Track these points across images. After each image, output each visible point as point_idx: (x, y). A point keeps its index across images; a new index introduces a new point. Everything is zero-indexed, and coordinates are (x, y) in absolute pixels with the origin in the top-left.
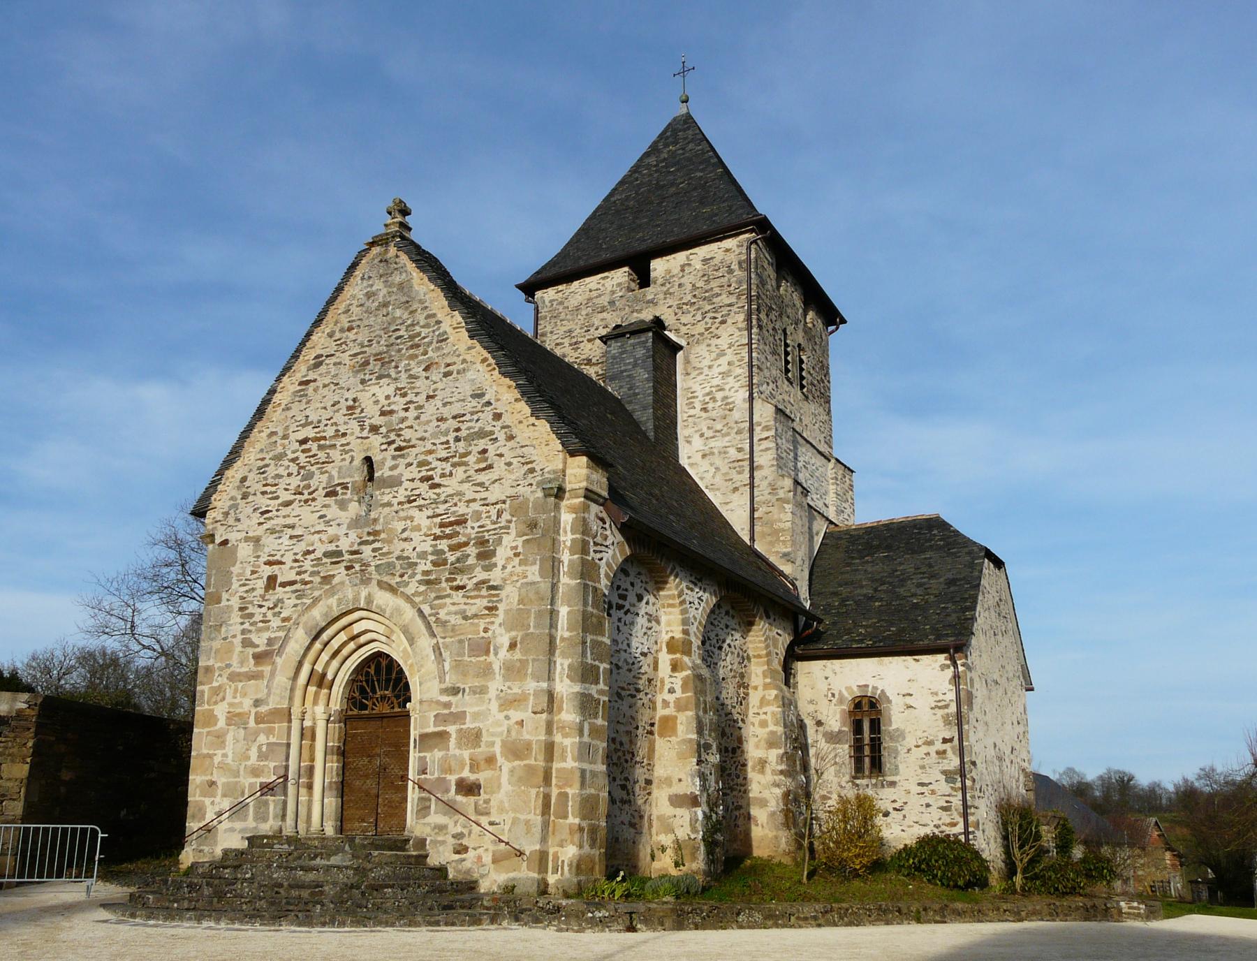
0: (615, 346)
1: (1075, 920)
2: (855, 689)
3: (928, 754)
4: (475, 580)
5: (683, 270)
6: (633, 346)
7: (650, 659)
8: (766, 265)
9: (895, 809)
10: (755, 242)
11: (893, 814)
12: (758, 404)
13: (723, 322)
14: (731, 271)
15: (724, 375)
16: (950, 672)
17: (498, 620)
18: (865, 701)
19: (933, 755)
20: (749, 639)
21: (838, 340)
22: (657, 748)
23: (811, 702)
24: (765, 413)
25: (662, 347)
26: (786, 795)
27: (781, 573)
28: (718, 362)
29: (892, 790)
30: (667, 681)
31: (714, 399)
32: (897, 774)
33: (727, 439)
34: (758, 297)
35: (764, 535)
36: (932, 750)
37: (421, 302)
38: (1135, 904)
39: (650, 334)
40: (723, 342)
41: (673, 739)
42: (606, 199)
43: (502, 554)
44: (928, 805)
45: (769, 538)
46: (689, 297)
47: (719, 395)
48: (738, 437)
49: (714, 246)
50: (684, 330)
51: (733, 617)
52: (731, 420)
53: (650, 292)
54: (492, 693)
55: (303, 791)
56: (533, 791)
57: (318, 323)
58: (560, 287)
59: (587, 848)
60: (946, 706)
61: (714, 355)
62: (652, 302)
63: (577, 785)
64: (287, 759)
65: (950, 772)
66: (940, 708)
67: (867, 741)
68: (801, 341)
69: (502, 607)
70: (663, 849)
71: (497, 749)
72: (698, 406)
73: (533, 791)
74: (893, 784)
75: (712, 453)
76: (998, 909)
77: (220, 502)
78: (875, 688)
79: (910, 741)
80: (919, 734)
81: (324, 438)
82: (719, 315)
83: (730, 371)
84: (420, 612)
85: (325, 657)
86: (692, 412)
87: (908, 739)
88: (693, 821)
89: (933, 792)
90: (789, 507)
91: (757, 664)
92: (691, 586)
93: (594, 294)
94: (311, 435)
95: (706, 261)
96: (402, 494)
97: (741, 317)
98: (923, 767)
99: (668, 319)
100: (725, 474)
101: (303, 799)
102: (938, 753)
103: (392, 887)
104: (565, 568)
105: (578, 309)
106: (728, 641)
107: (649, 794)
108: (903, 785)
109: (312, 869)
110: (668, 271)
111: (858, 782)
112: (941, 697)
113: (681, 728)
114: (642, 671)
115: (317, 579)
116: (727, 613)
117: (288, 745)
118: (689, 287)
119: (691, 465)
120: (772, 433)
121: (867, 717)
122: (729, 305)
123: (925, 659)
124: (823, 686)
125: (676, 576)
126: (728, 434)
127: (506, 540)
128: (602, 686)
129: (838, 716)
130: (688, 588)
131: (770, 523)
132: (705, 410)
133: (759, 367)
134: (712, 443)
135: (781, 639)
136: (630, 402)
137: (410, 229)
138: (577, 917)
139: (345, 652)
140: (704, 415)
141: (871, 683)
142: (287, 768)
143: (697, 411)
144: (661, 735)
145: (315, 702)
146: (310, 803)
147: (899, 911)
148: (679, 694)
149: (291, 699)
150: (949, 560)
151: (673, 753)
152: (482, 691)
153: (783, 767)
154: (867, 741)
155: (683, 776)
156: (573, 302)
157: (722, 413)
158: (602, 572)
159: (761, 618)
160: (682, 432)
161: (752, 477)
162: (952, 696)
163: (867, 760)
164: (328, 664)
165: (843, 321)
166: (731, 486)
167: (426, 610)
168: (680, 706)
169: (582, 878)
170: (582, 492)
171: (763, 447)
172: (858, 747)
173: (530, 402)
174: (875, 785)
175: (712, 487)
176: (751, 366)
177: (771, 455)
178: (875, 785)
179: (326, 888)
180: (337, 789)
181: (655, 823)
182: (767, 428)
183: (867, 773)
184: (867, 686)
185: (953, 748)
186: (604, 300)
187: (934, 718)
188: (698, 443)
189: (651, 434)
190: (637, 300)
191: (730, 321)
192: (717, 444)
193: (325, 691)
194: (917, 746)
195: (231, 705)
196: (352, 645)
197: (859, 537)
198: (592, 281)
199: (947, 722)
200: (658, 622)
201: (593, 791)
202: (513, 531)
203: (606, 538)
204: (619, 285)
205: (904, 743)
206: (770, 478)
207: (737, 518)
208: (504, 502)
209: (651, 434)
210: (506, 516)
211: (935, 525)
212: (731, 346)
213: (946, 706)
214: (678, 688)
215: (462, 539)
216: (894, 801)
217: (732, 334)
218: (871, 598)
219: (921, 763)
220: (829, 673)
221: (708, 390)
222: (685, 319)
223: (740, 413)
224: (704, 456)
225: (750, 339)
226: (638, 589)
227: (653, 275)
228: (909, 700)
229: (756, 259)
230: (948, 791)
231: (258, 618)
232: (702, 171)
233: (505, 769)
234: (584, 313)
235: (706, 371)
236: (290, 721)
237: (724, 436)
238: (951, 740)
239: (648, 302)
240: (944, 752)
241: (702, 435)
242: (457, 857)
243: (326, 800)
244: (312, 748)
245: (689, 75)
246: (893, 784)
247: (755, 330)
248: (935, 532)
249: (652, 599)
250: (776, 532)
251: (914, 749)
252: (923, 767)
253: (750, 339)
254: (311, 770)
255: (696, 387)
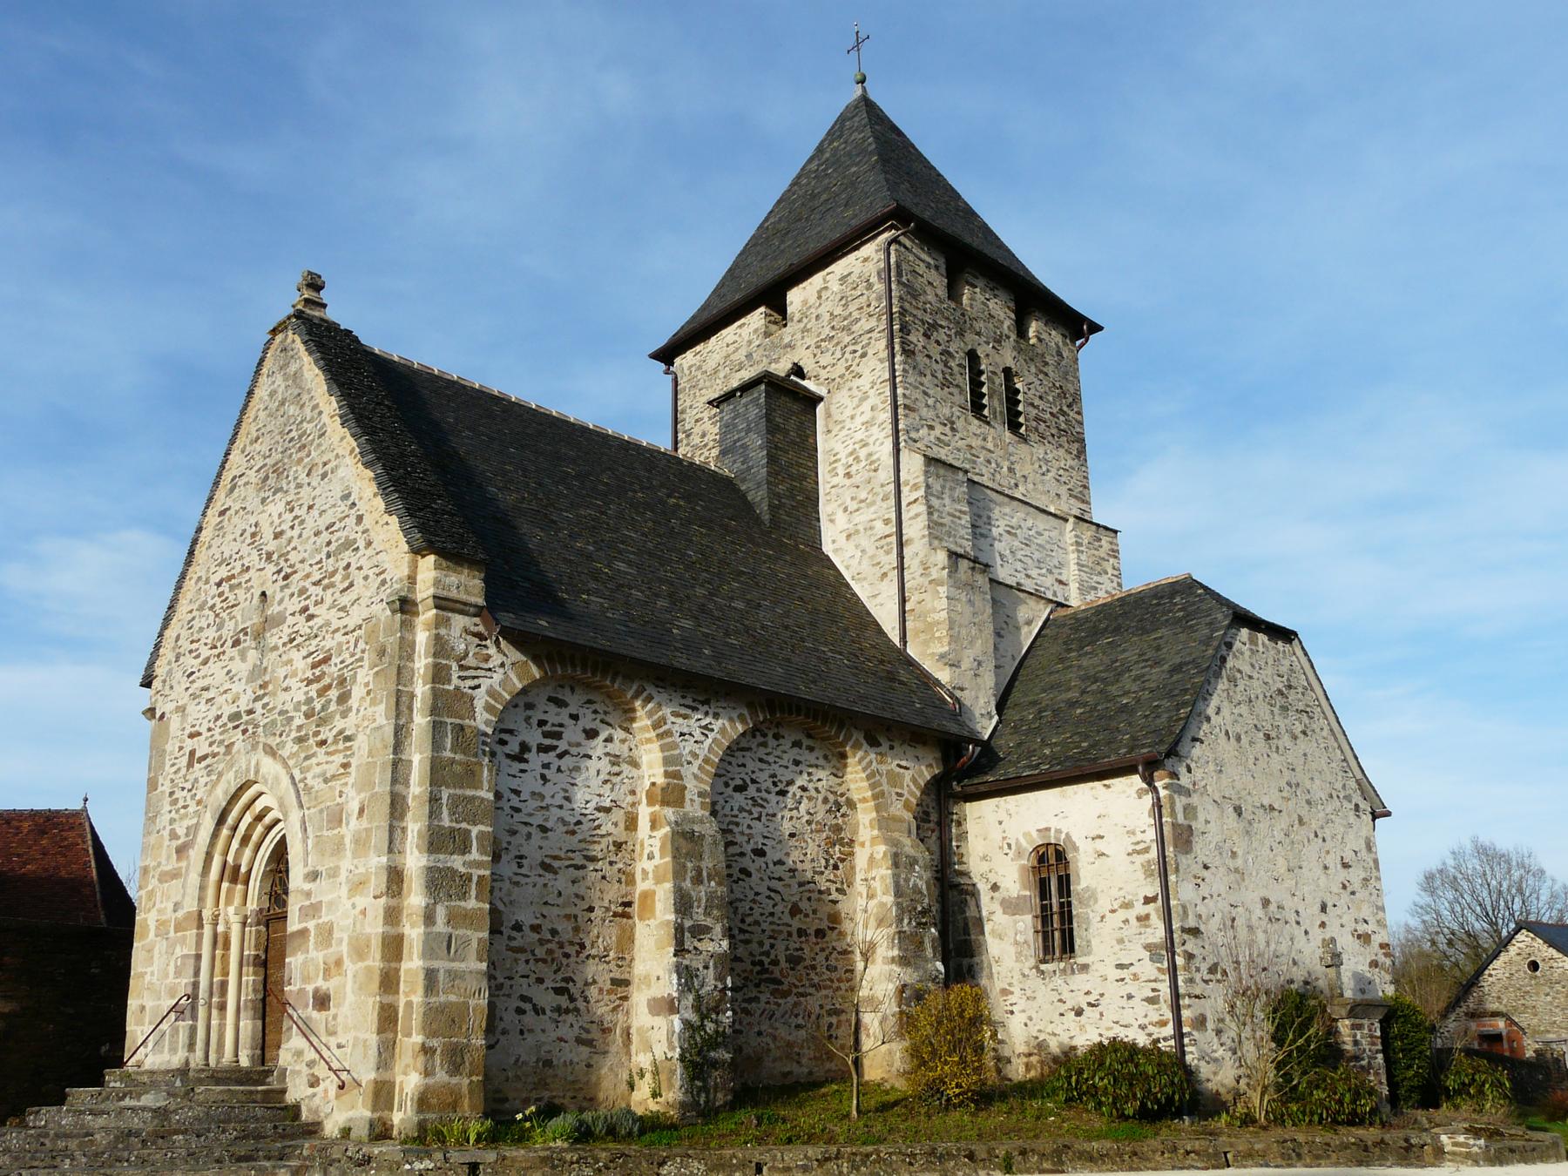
0: (726, 407)
1: (1337, 1164)
2: (1035, 834)
3: (1126, 921)
4: (334, 732)
5: (819, 297)
6: (746, 406)
7: (618, 815)
8: (921, 269)
9: (1090, 1004)
10: (895, 240)
11: (1088, 1011)
12: (905, 455)
13: (864, 355)
14: (870, 286)
15: (868, 424)
16: (1148, 799)
17: (351, 780)
18: (1051, 850)
19: (1133, 921)
20: (848, 777)
21: (1091, 353)
22: (637, 935)
23: (984, 858)
24: (913, 465)
25: (786, 404)
26: (903, 988)
27: (938, 683)
28: (861, 409)
29: (1084, 976)
30: (647, 842)
31: (857, 459)
32: (1089, 953)
33: (872, 509)
34: (903, 312)
35: (917, 632)
36: (1131, 914)
37: (309, 391)
38: (1461, 1139)
39: (763, 387)
40: (864, 382)
41: (652, 922)
42: (761, 226)
43: (357, 692)
44: (1130, 997)
45: (923, 637)
46: (827, 331)
47: (863, 453)
48: (884, 505)
49: (851, 258)
50: (824, 374)
51: (811, 749)
52: (875, 484)
53: (788, 334)
54: (343, 875)
55: (215, 1012)
56: (371, 1001)
57: (232, 441)
58: (698, 348)
59: (441, 1076)
60: (1146, 850)
61: (856, 400)
62: (790, 346)
63: (420, 991)
64: (197, 973)
65: (1155, 946)
66: (1138, 852)
67: (1055, 908)
68: (1010, 363)
69: (354, 762)
70: (642, 1075)
71: (344, 948)
72: (841, 471)
73: (371, 1001)
74: (1085, 968)
75: (857, 532)
76: (1175, 1149)
77: (161, 669)
78: (1058, 831)
79: (1103, 905)
80: (1115, 893)
81: (233, 576)
82: (858, 347)
83: (873, 418)
84: (292, 778)
85: (235, 844)
86: (835, 481)
87: (1100, 902)
88: (671, 1033)
89: (1135, 977)
90: (943, 590)
91: (865, 810)
92: (683, 711)
93: (732, 348)
94: (225, 575)
95: (843, 279)
96: (286, 631)
97: (883, 343)
98: (1120, 941)
99: (808, 365)
100: (872, 557)
101: (214, 1022)
102: (1139, 919)
103: (184, 1132)
104: (417, 704)
105: (716, 371)
106: (799, 783)
107: (625, 998)
108: (1098, 969)
109: (103, 1112)
110: (805, 302)
111: (1043, 967)
112: (1139, 837)
113: (659, 906)
114: (603, 831)
115: (222, 750)
116: (797, 744)
117: (198, 957)
118: (827, 317)
119: (836, 551)
120: (921, 492)
121: (1051, 868)
122: (871, 331)
123: (1118, 783)
124: (996, 835)
125: (649, 699)
126: (873, 503)
127: (361, 674)
128: (475, 855)
129: (1016, 876)
130: (675, 714)
131: (922, 616)
132: (848, 475)
133: (906, 407)
134: (857, 518)
135: (908, 775)
136: (744, 480)
137: (324, 306)
138: (390, 1169)
139: (255, 837)
140: (847, 482)
141: (1054, 824)
142: (196, 985)
143: (839, 480)
144: (641, 919)
145: (229, 902)
146: (222, 1027)
147: (971, 1156)
148: (657, 861)
149: (201, 899)
150: (1182, 637)
151: (652, 941)
152: (334, 873)
153: (896, 952)
154: (1055, 908)
155: (661, 973)
156: (710, 365)
157: (867, 475)
158: (479, 705)
159: (857, 746)
160: (824, 509)
161: (901, 557)
162: (1151, 834)
163: (1057, 934)
164: (239, 853)
165: (1095, 328)
166: (878, 572)
167: (298, 777)
168: (659, 880)
169: (431, 1116)
170: (430, 601)
171: (912, 514)
172: (1045, 916)
173: (385, 495)
174: (1064, 971)
175: (858, 576)
176: (895, 407)
177: (922, 521)
178: (1064, 971)
179: (97, 1136)
180: (254, 1009)
181: (635, 1038)
182: (915, 487)
183: (1057, 954)
184: (1048, 829)
185: (1157, 910)
186: (741, 355)
187: (1132, 868)
188: (841, 519)
189: (766, 517)
190: (774, 346)
191: (870, 352)
192: (862, 518)
193: (240, 887)
194: (1113, 911)
195: (159, 911)
196: (260, 829)
197: (1087, 619)
198: (728, 333)
199: (1148, 874)
200: (635, 764)
201: (453, 998)
202: (366, 663)
203: (487, 658)
204: (756, 331)
205: (1096, 907)
206: (921, 555)
207: (885, 614)
208: (360, 627)
209: (766, 517)
210: (361, 645)
211: (1188, 586)
212: (874, 384)
213: (1146, 850)
214: (657, 854)
215: (327, 681)
216: (1088, 993)
217: (874, 369)
218: (1072, 704)
219: (1118, 935)
220: (1002, 816)
221: (850, 448)
222: (825, 360)
223: (886, 474)
224: (849, 537)
225: (893, 371)
226: (587, 721)
227: (789, 310)
228: (1100, 845)
229: (898, 266)
230: (1154, 974)
231: (181, 803)
232: (857, 165)
233: (350, 974)
234: (722, 375)
235: (848, 424)
236: (200, 926)
237: (870, 505)
238: (1154, 899)
239: (787, 346)
240: (1147, 917)
241: (846, 510)
242: (311, 1090)
243: (242, 1024)
244: (225, 958)
245: (864, 47)
246: (1085, 968)
247: (898, 358)
248: (1177, 599)
249: (619, 734)
250: (930, 627)
251: (1109, 915)
252: (1120, 941)
253: (893, 371)
254: (224, 985)
255: (839, 447)
